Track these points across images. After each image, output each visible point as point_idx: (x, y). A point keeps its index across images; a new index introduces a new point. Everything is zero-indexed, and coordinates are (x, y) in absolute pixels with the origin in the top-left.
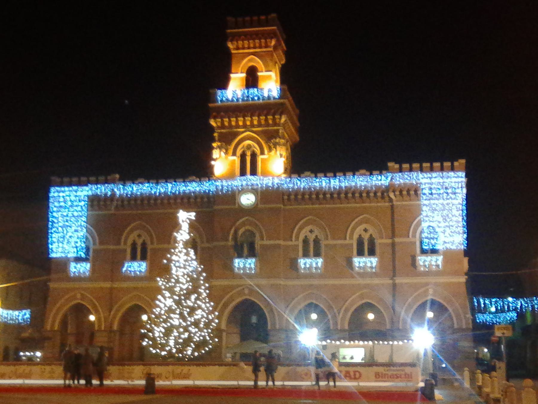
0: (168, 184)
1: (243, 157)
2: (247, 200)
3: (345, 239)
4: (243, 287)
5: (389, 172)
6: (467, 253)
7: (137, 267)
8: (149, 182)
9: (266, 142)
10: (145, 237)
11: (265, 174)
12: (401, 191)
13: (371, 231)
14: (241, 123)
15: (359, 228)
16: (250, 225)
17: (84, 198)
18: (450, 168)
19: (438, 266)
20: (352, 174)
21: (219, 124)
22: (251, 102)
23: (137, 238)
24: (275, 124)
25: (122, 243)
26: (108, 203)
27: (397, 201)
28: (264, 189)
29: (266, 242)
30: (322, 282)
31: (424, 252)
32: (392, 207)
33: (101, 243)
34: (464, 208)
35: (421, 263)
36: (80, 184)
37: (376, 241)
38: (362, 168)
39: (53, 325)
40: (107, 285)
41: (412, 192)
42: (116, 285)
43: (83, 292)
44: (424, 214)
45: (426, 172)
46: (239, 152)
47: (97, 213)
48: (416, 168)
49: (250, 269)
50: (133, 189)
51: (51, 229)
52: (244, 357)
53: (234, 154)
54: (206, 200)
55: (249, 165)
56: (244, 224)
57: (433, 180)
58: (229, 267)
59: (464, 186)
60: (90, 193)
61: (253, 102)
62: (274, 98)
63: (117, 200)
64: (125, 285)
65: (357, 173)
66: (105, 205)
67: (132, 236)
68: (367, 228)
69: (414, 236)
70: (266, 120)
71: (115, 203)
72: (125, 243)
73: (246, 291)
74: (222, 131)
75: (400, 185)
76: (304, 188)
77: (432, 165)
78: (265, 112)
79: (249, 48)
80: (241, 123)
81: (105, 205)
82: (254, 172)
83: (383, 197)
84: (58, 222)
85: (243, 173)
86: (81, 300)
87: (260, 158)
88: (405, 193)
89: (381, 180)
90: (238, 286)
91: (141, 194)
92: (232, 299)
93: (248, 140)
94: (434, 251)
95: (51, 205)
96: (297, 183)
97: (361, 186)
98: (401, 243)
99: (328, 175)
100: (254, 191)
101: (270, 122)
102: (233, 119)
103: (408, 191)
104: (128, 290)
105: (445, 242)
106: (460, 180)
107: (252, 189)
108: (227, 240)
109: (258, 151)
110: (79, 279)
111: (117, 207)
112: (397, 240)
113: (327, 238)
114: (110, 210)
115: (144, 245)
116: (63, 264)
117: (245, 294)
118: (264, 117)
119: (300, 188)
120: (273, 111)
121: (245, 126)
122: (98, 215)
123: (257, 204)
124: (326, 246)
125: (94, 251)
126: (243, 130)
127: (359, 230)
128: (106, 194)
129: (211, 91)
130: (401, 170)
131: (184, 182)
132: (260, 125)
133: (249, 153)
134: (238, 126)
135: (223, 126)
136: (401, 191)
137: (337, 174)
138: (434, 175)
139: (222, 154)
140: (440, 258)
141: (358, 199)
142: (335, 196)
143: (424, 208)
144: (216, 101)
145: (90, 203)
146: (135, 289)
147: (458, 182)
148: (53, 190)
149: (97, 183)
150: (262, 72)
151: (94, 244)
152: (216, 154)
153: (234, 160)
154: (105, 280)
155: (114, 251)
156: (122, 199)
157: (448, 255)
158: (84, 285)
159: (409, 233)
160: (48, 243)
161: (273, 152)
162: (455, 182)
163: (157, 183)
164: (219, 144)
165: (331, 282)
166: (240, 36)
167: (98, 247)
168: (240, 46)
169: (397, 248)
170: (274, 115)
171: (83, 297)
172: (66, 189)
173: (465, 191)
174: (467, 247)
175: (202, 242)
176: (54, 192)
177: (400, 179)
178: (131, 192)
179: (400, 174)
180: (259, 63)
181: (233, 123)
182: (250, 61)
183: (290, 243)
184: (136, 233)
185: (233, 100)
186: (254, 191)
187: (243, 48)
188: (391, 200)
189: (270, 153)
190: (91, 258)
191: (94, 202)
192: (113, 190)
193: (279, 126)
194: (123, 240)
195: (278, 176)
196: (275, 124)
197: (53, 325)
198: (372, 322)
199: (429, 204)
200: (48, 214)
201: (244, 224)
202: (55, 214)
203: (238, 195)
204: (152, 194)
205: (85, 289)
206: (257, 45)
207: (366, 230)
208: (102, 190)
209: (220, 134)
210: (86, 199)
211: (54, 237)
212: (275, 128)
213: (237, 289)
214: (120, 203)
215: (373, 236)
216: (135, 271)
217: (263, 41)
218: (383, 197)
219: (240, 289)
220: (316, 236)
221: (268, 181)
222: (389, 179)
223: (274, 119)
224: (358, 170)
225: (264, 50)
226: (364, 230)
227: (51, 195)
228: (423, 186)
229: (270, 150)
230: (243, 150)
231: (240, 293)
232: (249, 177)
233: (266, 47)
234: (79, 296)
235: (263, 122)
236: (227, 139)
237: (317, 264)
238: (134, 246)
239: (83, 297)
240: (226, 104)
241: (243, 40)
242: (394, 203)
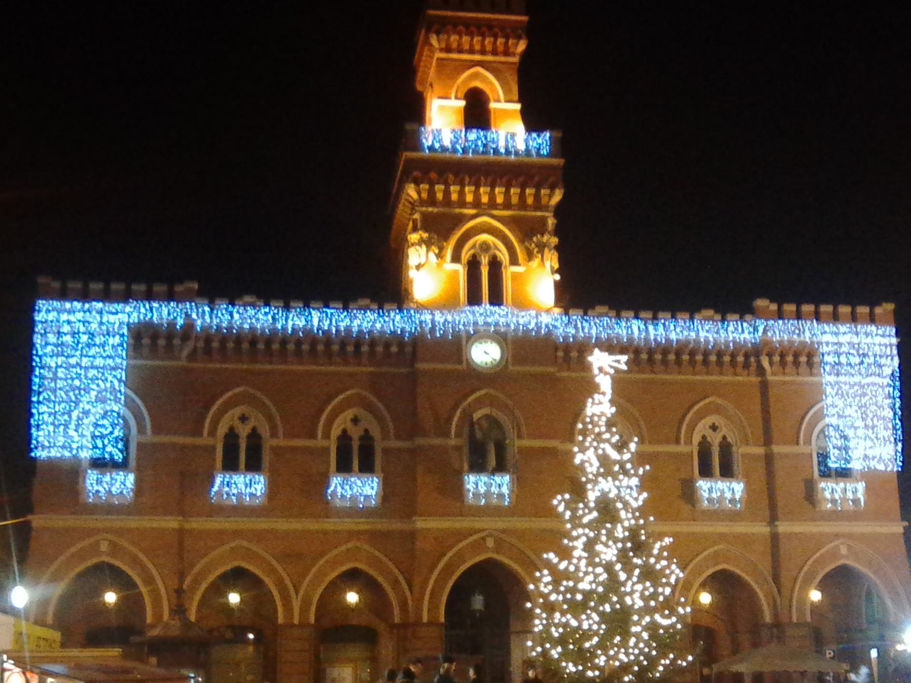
0: (313, 312)
1: (473, 266)
2: (484, 354)
3: (677, 441)
4: (485, 534)
5: (760, 318)
6: (901, 475)
7: (486, 487)
8: (267, 304)
9: (522, 241)
10: (258, 421)
11: (521, 304)
12: (782, 356)
13: (258, 421)
14: (469, 198)
15: (703, 421)
16: (491, 405)
17: (120, 327)
18: (794, 315)
19: (856, 501)
20: (687, 316)
21: (424, 195)
22: (491, 157)
23: (237, 423)
24: (538, 206)
26: (177, 342)
27: (773, 374)
28: (520, 333)
29: (526, 443)
31: (826, 473)
32: (764, 387)
33: (157, 430)
34: (897, 394)
35: (828, 495)
36: (106, 296)
37: (734, 449)
38: (707, 307)
40: (172, 523)
41: (803, 359)
42: (195, 524)
44: (829, 401)
45: (843, 323)
46: (466, 255)
47: (149, 362)
48: (827, 313)
49: (501, 496)
50: (232, 316)
51: (39, 393)
53: (456, 259)
54: (394, 349)
55: (485, 283)
56: (479, 403)
57: (843, 339)
58: (458, 490)
59: (895, 352)
60: (134, 318)
61: (496, 157)
62: (517, 153)
63: (197, 338)
65: (697, 316)
66: (169, 347)
67: (228, 419)
68: (717, 424)
69: (808, 442)
70: (522, 196)
71: (190, 344)
72: (213, 433)
73: (490, 543)
74: (430, 209)
75: (781, 342)
76: (360, 331)
77: (86, 286)
78: (521, 179)
79: (471, 51)
80: (469, 198)
81: (169, 347)
82: (496, 299)
83: (746, 366)
84: (55, 379)
85: (474, 298)
86: (108, 555)
87: (509, 272)
88: (790, 358)
89: (738, 332)
90: (473, 532)
91: (252, 329)
93: (488, 233)
94: (844, 474)
95: (38, 340)
96: (583, 328)
97: (707, 341)
98: (787, 456)
99: (643, 314)
100: (500, 337)
101: (530, 201)
102: (439, 188)
103: (796, 355)
104: (221, 536)
105: (866, 457)
106: (886, 340)
107: (495, 332)
108: (447, 435)
109: (504, 256)
110: (108, 508)
111: (192, 356)
112: (776, 449)
113: (274, 434)
114: (179, 359)
115: (725, 447)
116: (67, 475)
117: (487, 549)
118: (518, 190)
119: (590, 338)
120: (537, 179)
121: (477, 204)
122: (140, 367)
123: (506, 366)
124: (385, 451)
125: (141, 446)
126: (472, 212)
128: (172, 324)
129: (409, 127)
130: (780, 315)
131: (346, 308)
132: (507, 205)
133: (485, 260)
134: (462, 203)
135: (432, 200)
136: (782, 356)
137: (292, 304)
138: (843, 328)
139: (432, 256)
140: (861, 486)
141: (727, 366)
142: (658, 357)
143: (829, 390)
144: (417, 145)
145: (132, 341)
147: (886, 346)
148: (41, 304)
149: (149, 296)
150: (499, 101)
151: (141, 430)
152: (416, 255)
153: (456, 272)
154: (167, 512)
155: (183, 447)
156: (207, 337)
157: (871, 478)
158: (117, 522)
159: (798, 437)
160: (29, 426)
161: (536, 262)
162: (880, 345)
163: (287, 308)
164: (425, 235)
165: (282, 525)
166: (455, 26)
167: (149, 437)
168: (454, 45)
169: (779, 465)
170: (538, 187)
171: (115, 549)
172: (77, 305)
173: (896, 361)
174: (902, 467)
175: (385, 437)
176: (46, 312)
177: (781, 331)
178: (230, 322)
179: (781, 322)
180: (491, 83)
181: (454, 197)
182: (476, 76)
183: (198, 441)
185: (455, 150)
186: (500, 337)
187: (460, 51)
188: (761, 371)
189: (530, 264)
190: (132, 462)
191: (143, 338)
192: (188, 316)
193: (547, 211)
195: (548, 311)
196: (538, 205)
197: (158, 616)
198: (353, 610)
199: (837, 383)
200: (32, 360)
201: (479, 403)
202: (47, 360)
203: (467, 342)
204: (275, 329)
205: (120, 532)
206: (489, 48)
207: (714, 428)
208: (163, 313)
209: (425, 217)
210: (125, 331)
211: (42, 412)
212: (539, 214)
213: (471, 539)
214: (201, 344)
215: (729, 440)
216: (239, 495)
217: (500, 41)
218: (746, 366)
219: (476, 537)
220: (724, 438)
221: (525, 320)
222: (761, 329)
223: (537, 197)
224: (355, 299)
225: (503, 59)
226: (710, 427)
227: (38, 317)
228: (825, 349)
229: (530, 256)
230: (472, 252)
231: (479, 546)
232: (486, 307)
233: (506, 53)
234: (104, 546)
235: (515, 200)
236: (440, 228)
237: (855, 492)
238: (231, 438)
240: (440, 155)
241: (460, 34)
242: (770, 378)
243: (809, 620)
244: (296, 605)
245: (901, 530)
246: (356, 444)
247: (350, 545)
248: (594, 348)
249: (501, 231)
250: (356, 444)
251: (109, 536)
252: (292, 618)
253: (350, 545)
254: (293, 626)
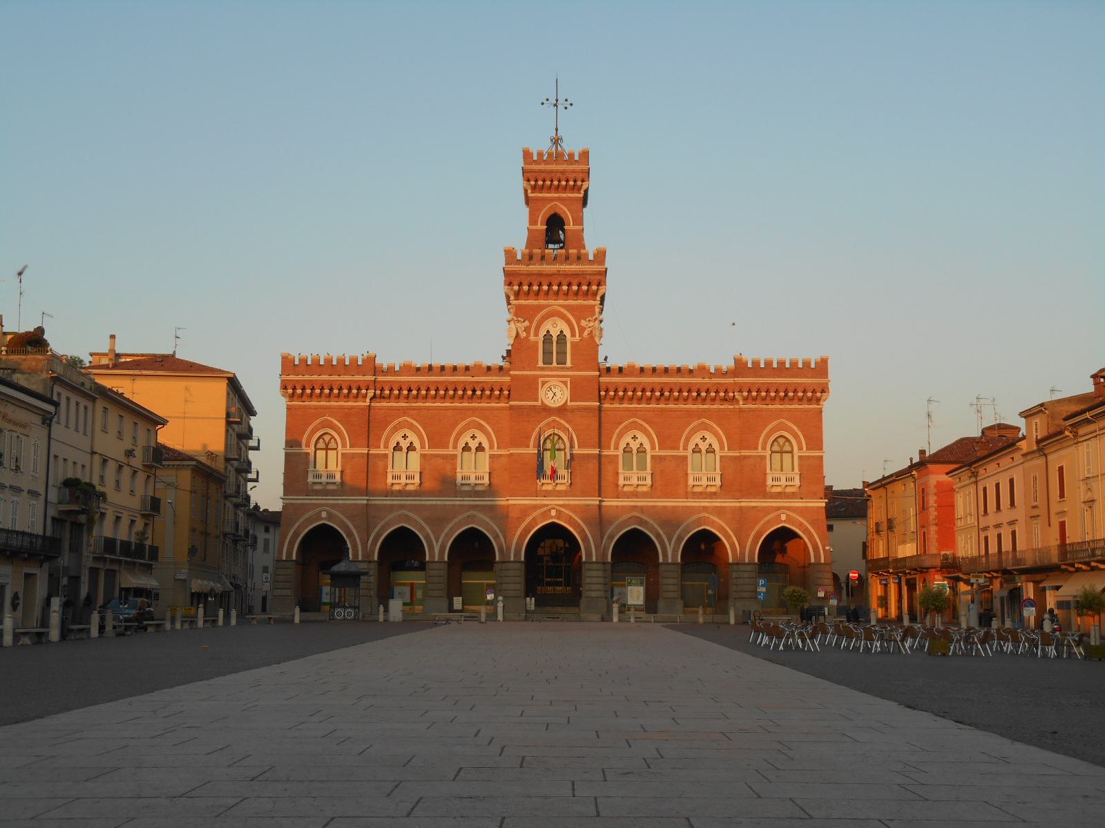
4: (549, 507)
25: (382, 446)
30: (717, 503)
39: (289, 553)
43: (791, 514)
52: (1083, 607)
64: (388, 501)
73: (553, 513)
92: (388, 525)
104: (392, 508)
127: (627, 439)
146: (402, 507)
171: (330, 516)
184: (469, 433)
194: (681, 445)
205: (333, 506)
231: (546, 514)
239: (330, 516)
243: (1032, 598)
244: (437, 551)
245: (824, 505)
246: (555, 339)
247: (469, 513)
248: (329, 574)
249: (490, 434)
250: (555, 339)
251: (788, 512)
252: (434, 558)
253: (469, 513)
254: (434, 562)
